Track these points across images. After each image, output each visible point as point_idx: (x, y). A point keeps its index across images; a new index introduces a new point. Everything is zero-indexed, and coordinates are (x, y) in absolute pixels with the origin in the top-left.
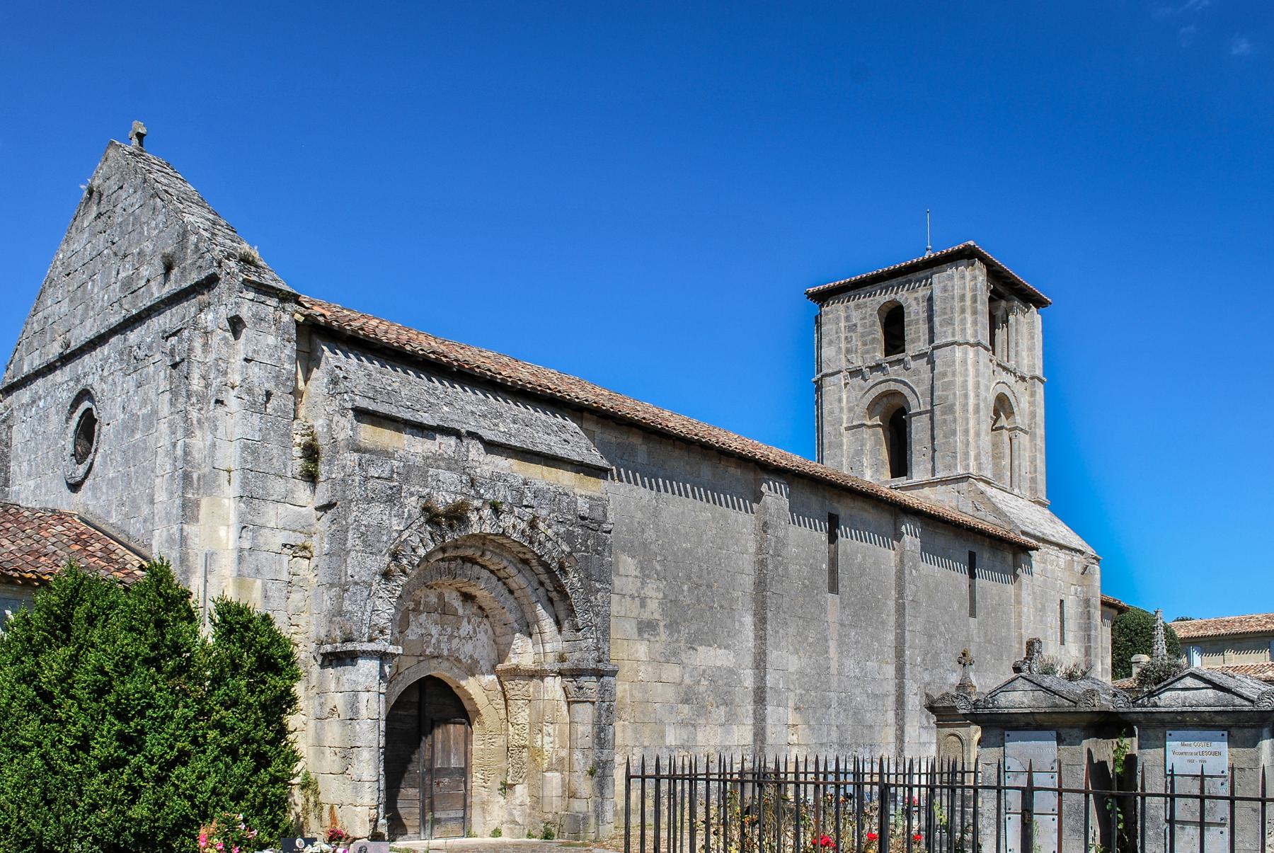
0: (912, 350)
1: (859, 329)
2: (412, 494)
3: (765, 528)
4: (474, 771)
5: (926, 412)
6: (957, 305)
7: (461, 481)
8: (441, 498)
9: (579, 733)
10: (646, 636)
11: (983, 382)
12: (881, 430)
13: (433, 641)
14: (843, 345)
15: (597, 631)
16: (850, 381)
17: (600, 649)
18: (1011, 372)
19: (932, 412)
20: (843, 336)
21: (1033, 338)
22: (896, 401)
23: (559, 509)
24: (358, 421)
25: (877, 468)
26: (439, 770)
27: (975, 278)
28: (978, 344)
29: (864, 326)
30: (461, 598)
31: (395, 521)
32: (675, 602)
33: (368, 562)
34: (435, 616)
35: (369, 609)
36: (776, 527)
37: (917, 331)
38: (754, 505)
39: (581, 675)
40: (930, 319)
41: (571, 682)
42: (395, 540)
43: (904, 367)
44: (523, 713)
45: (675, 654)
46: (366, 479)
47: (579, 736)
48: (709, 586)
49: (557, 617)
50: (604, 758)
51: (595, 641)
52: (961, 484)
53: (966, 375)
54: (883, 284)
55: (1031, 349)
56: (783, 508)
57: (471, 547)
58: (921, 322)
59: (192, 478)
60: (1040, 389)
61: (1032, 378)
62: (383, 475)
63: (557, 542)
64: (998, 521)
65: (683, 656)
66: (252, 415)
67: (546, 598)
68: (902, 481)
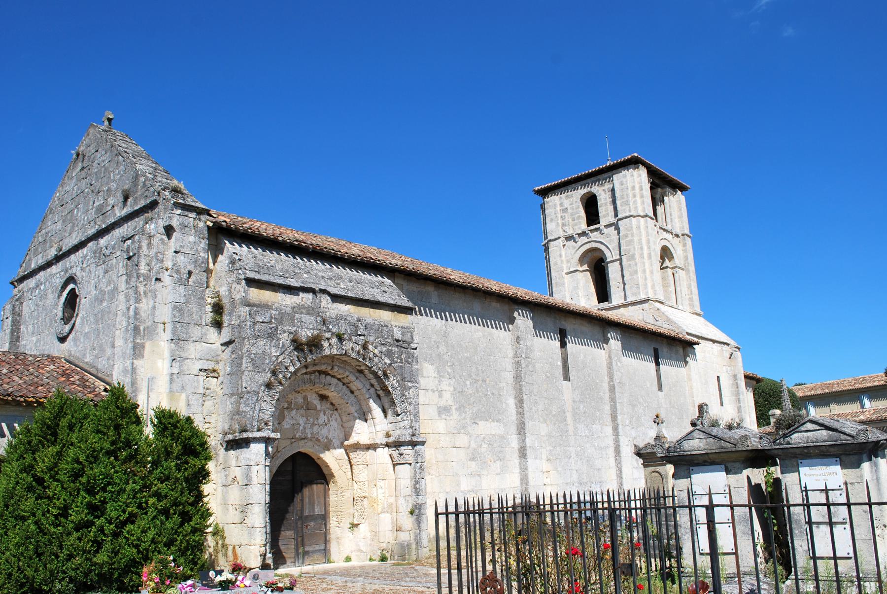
0: (604, 221)
1: (570, 211)
2: (284, 332)
3: (518, 341)
4: (331, 516)
5: (617, 260)
6: (630, 192)
7: (317, 321)
8: (304, 333)
9: (402, 485)
10: (443, 416)
11: (651, 239)
12: (588, 273)
13: (301, 428)
14: (560, 221)
15: (410, 415)
16: (566, 243)
17: (413, 427)
18: (669, 232)
19: (620, 260)
20: (559, 216)
21: (681, 210)
22: (597, 254)
23: (382, 335)
24: (249, 287)
25: (588, 296)
26: (307, 517)
27: (640, 175)
28: (646, 216)
29: (572, 208)
30: (319, 398)
31: (273, 349)
32: (461, 392)
33: (257, 378)
34: (302, 411)
35: (257, 409)
36: (525, 339)
37: (607, 210)
38: (510, 326)
39: (401, 446)
40: (614, 202)
41: (395, 450)
42: (274, 362)
43: (600, 233)
44: (363, 474)
45: (464, 427)
46: (254, 323)
47: (402, 488)
48: (484, 381)
49: (383, 407)
50: (419, 502)
51: (410, 422)
52: (644, 305)
53: (640, 236)
54: (582, 182)
55: (680, 217)
56: (529, 327)
57: (324, 364)
58: (608, 204)
59: (139, 329)
60: (689, 241)
61: (683, 235)
62: (265, 320)
63: (381, 358)
64: (670, 327)
65: (469, 429)
66: (179, 287)
67: (375, 395)
68: (605, 305)
